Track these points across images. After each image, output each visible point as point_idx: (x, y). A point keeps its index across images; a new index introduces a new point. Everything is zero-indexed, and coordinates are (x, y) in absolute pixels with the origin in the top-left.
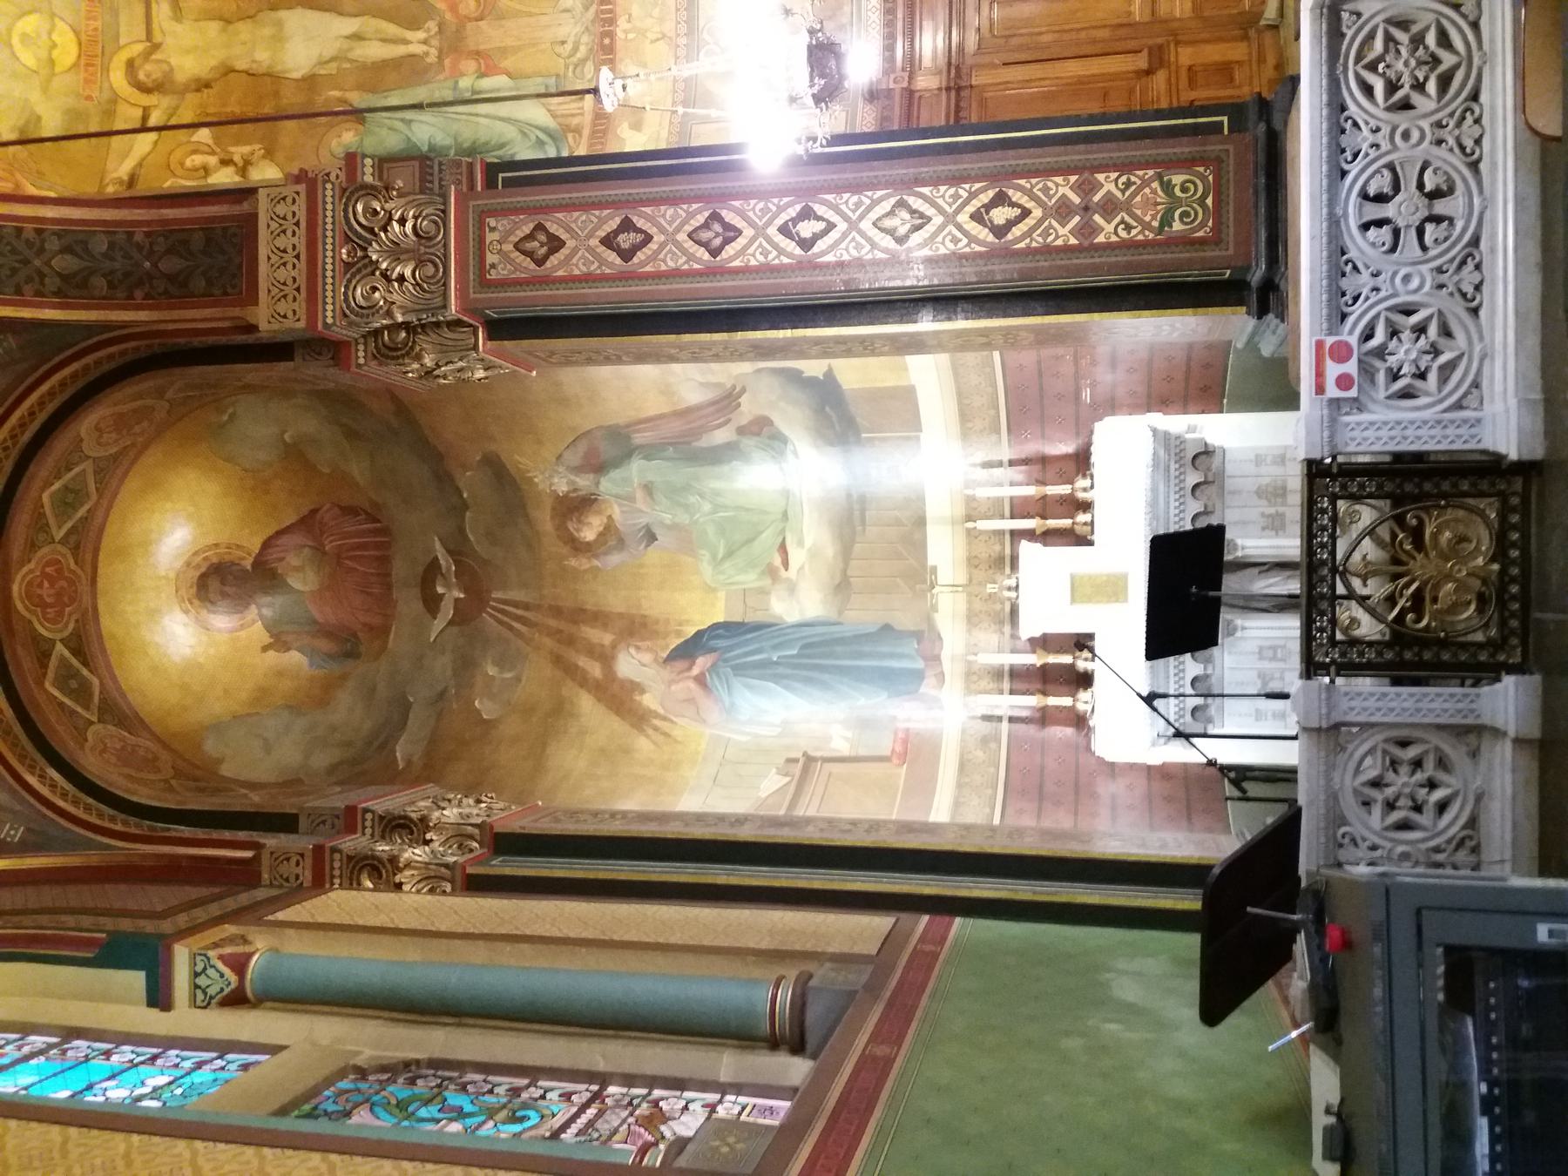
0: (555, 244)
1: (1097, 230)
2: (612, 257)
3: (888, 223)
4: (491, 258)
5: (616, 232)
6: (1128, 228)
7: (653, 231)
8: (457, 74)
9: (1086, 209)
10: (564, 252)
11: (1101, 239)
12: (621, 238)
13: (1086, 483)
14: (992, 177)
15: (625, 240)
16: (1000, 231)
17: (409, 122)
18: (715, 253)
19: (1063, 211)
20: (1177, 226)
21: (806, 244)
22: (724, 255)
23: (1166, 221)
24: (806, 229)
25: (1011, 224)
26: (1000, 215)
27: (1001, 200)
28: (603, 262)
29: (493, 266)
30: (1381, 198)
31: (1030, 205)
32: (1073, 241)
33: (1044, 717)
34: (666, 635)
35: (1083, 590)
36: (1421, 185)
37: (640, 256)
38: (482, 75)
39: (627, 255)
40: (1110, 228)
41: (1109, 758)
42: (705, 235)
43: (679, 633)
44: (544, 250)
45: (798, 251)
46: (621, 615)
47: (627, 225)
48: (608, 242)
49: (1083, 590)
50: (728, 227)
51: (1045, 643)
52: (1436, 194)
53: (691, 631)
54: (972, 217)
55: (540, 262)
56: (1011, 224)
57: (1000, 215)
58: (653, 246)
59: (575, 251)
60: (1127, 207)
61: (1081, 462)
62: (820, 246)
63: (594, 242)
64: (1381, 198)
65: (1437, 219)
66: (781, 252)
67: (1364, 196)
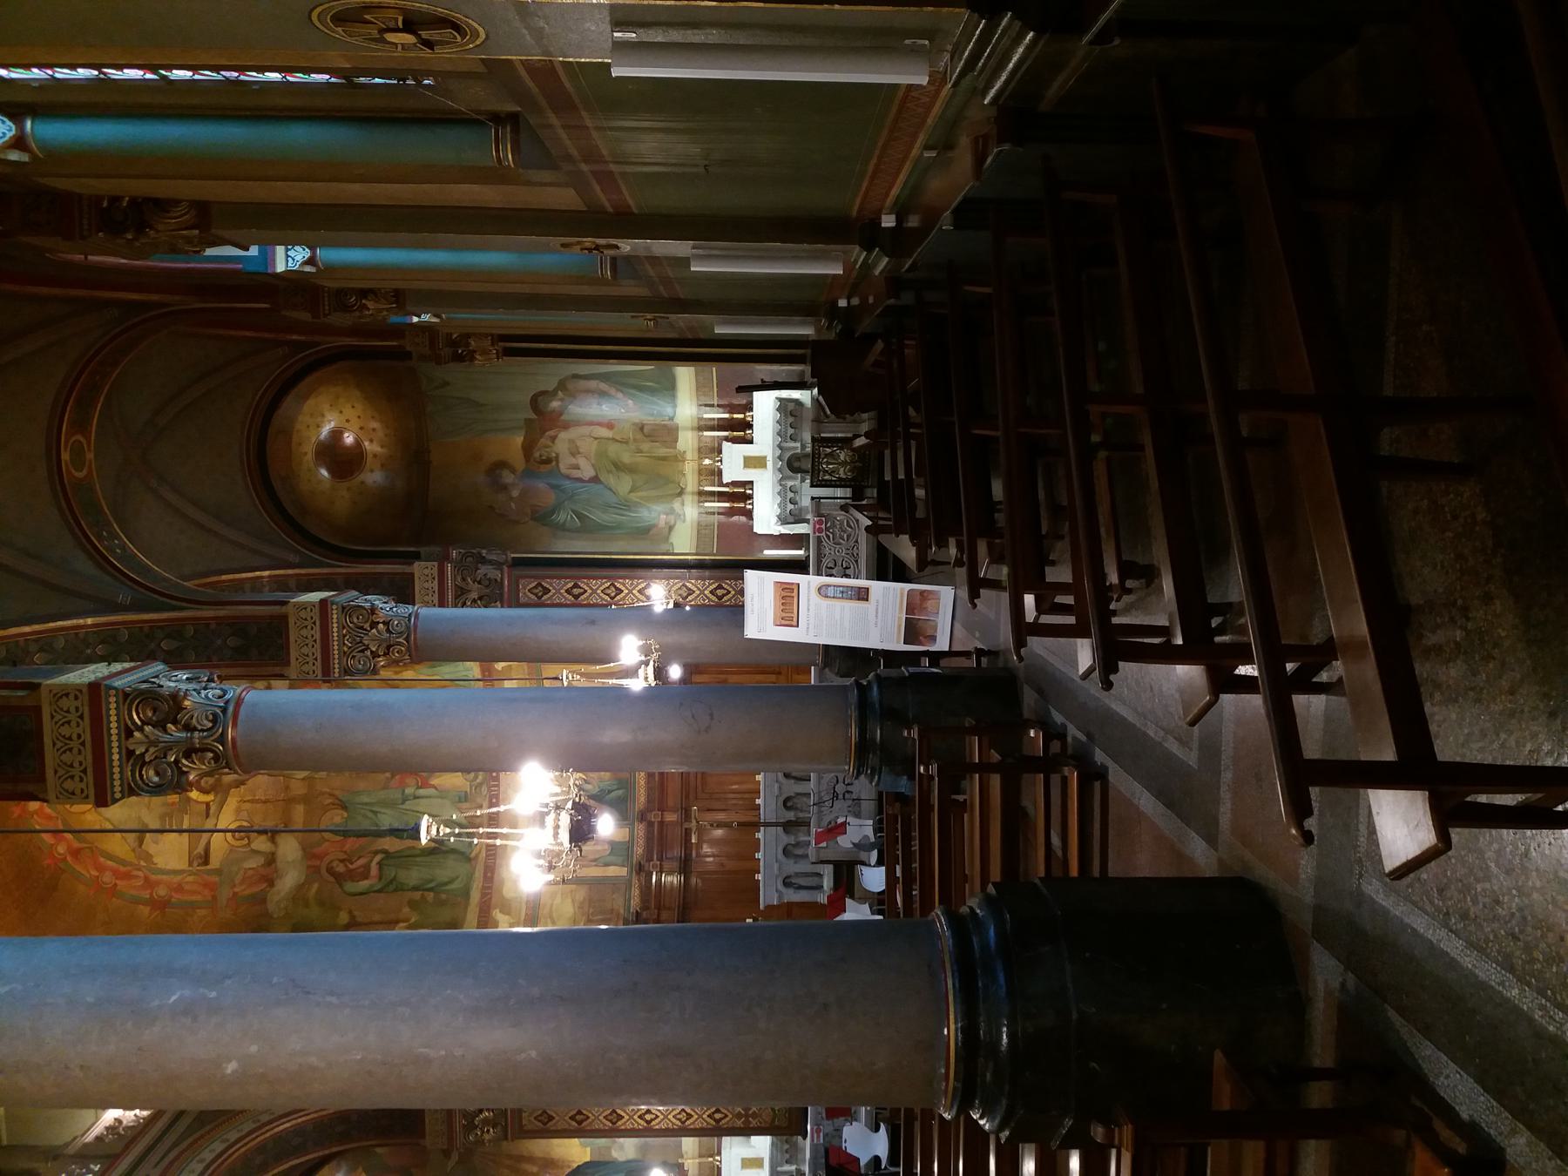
0: (546, 591)
1: (750, 1122)
2: (574, 1123)
3: (678, 1116)
4: (524, 1122)
5: (572, 588)
6: (761, 1123)
7: (590, 1115)
8: (403, 785)
9: (747, 1116)
10: (554, 1121)
11: (752, 1126)
12: (577, 1117)
13: (751, 432)
14: (717, 580)
15: (576, 591)
16: (718, 1121)
17: (375, 813)
18: (614, 1123)
19: (739, 1116)
20: (776, 1123)
21: (648, 1122)
22: (617, 1125)
23: (773, 1121)
24: (576, 591)
25: (724, 595)
26: (720, 592)
27: (720, 587)
28: (570, 1125)
29: (525, 1125)
30: (831, 568)
31: (731, 590)
32: (742, 1126)
33: (730, 512)
34: (562, 1168)
35: (750, 462)
36: (842, 565)
37: (584, 1124)
38: (419, 788)
39: (580, 1123)
40: (754, 1122)
41: (759, 533)
42: (609, 592)
43: (569, 1167)
44: (546, 1120)
45: (645, 1124)
46: (540, 1158)
47: (576, 586)
48: (572, 1118)
49: (750, 462)
50: (617, 589)
51: (734, 484)
52: (847, 568)
53: (575, 1165)
54: (708, 1116)
55: (545, 1124)
56: (724, 595)
57: (720, 592)
58: (590, 1120)
59: (558, 1121)
60: (761, 1116)
61: (749, 407)
62: (653, 1123)
63: (567, 1118)
64: (831, 568)
65: (848, 792)
66: (639, 1124)
67: (827, 567)
